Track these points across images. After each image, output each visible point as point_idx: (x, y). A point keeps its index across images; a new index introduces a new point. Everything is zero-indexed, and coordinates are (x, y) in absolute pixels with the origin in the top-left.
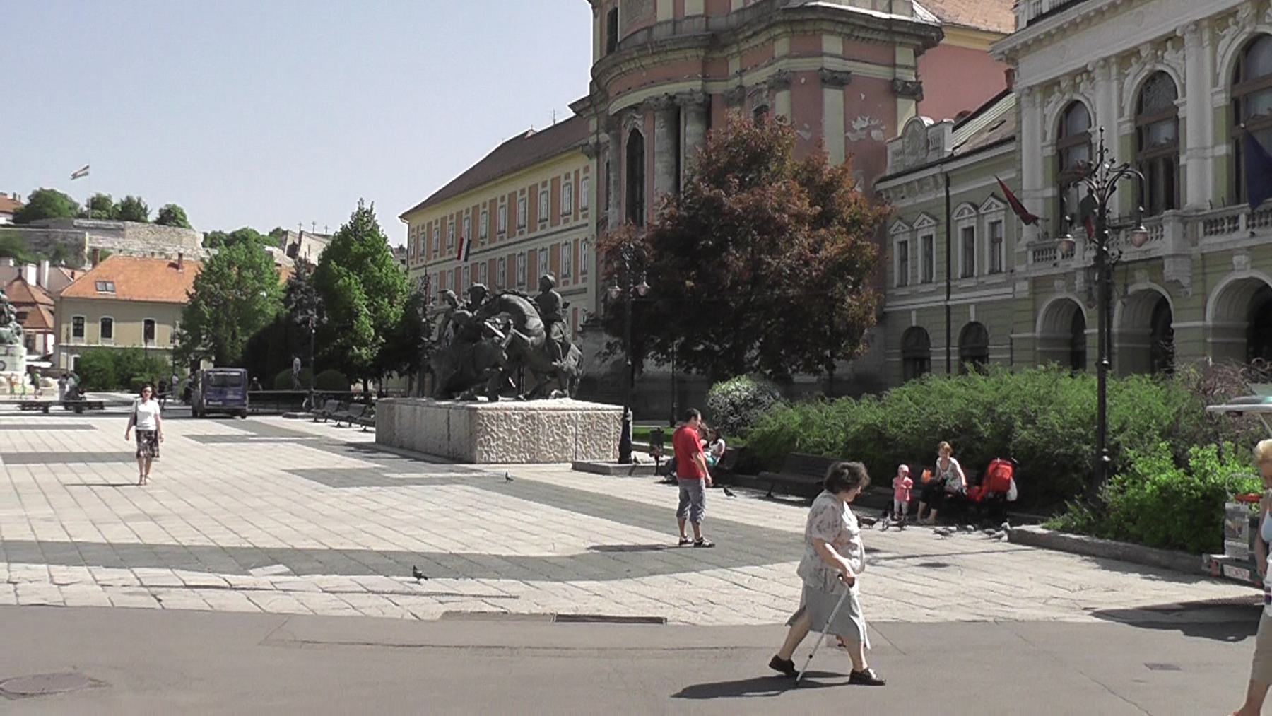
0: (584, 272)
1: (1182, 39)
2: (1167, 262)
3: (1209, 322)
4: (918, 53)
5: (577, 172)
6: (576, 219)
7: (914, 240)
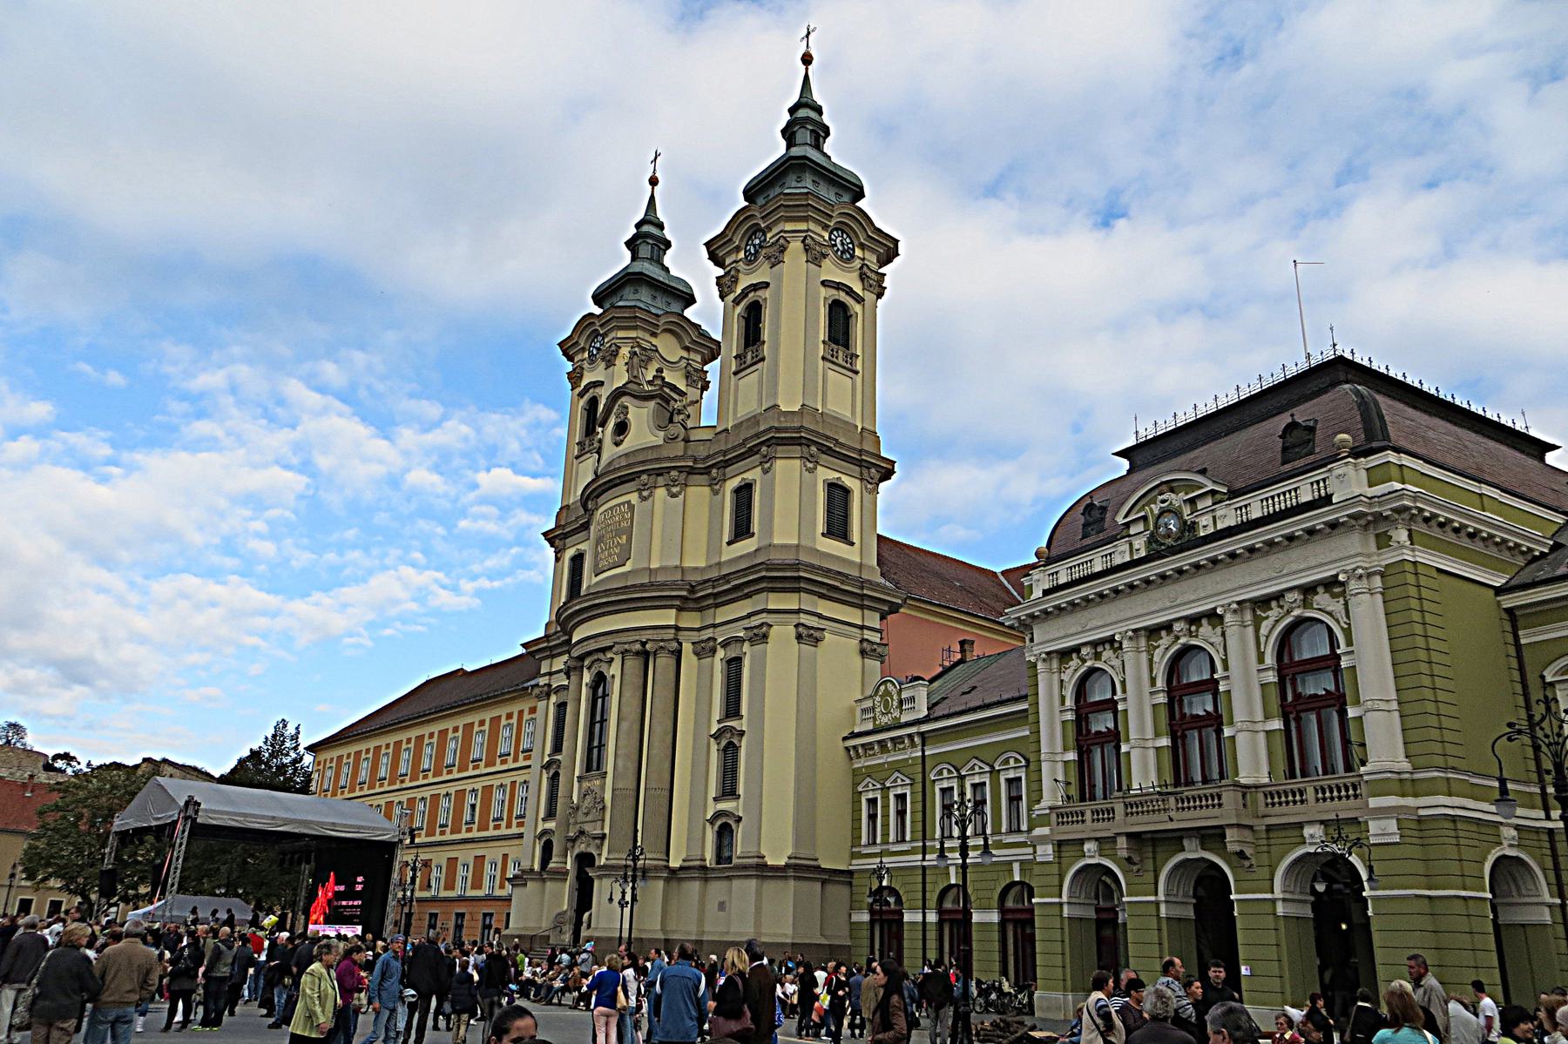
0: (522, 816)
1: (1221, 617)
2: (1228, 832)
3: (1065, 899)
4: (883, 618)
5: (521, 713)
6: (516, 760)
7: (886, 798)
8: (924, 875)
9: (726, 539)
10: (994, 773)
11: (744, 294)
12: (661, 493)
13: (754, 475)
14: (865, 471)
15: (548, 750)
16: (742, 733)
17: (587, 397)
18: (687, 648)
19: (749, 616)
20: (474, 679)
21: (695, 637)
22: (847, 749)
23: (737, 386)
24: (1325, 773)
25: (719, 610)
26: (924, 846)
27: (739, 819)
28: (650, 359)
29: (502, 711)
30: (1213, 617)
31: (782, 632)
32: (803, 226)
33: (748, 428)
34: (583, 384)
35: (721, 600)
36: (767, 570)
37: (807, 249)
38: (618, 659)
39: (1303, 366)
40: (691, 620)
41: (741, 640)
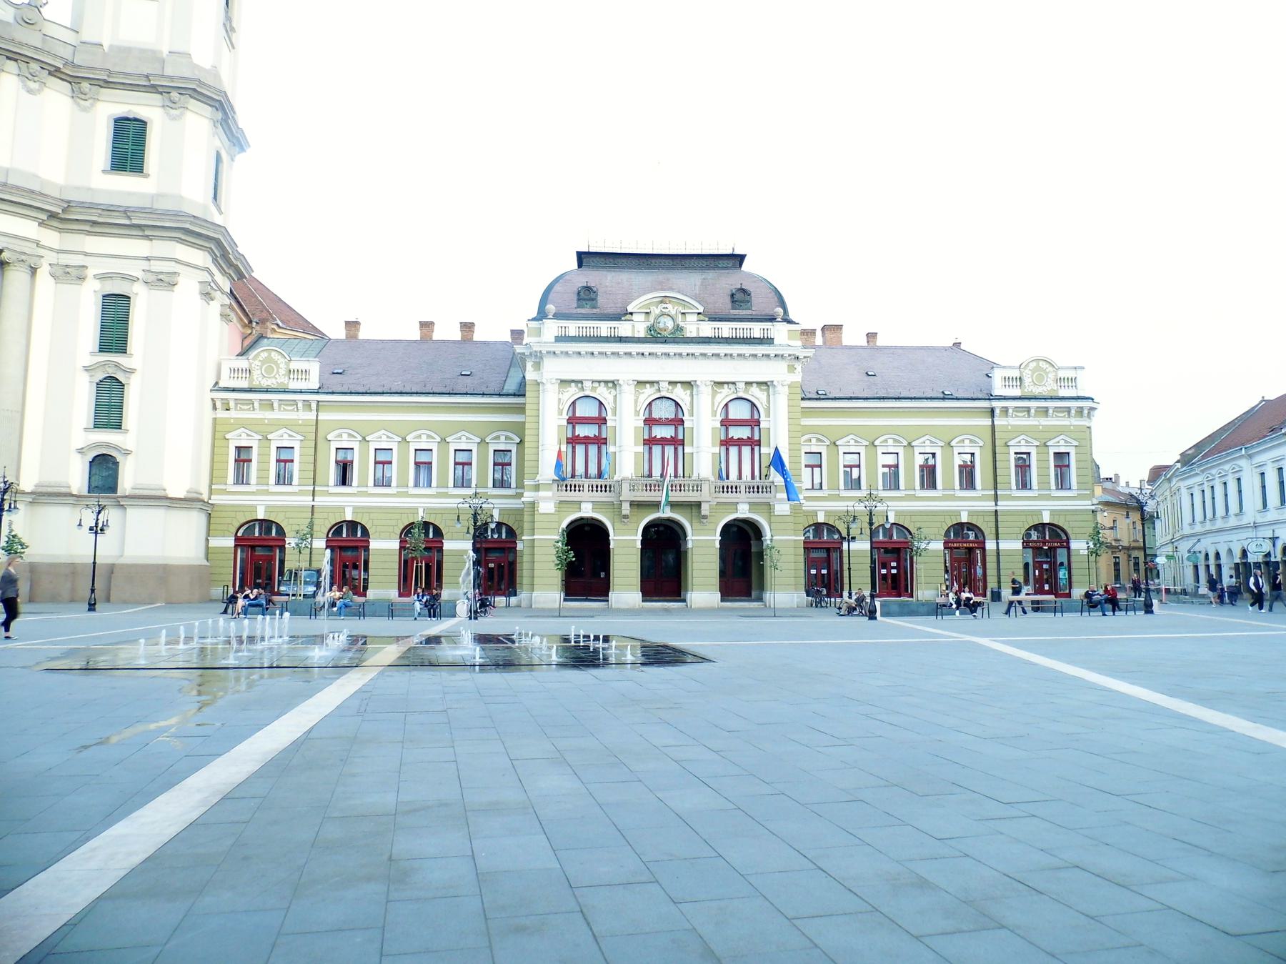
16: (131, 371)
24: (278, 483)
26: (996, 495)
30: (614, 384)
36: (191, 223)
39: (729, 252)
40: (50, 237)
41: (133, 279)
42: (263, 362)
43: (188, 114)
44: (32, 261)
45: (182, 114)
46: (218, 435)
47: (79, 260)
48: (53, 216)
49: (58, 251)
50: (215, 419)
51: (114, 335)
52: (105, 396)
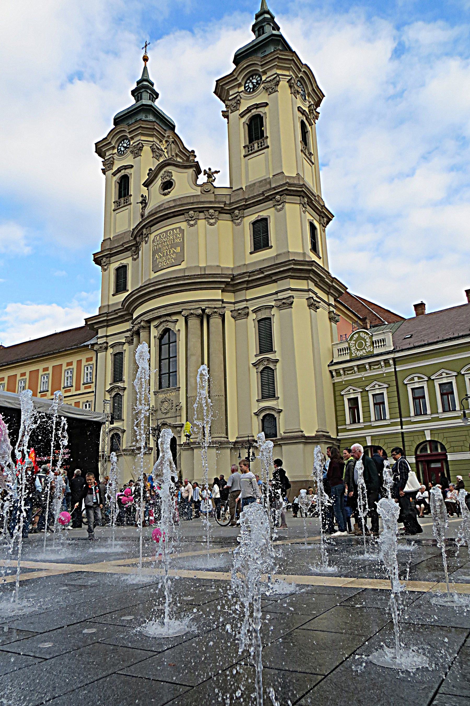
5: (79, 362)
6: (78, 389)
8: (403, 437)
9: (112, 293)
10: (365, 392)
11: (119, 171)
12: (202, 223)
13: (128, 261)
14: (321, 219)
15: (109, 379)
16: (277, 361)
17: (119, 175)
18: (228, 314)
19: (276, 293)
20: (8, 350)
21: (232, 307)
22: (331, 372)
23: (247, 165)
25: (109, 328)
26: (401, 421)
27: (124, 431)
28: (161, 155)
29: (63, 361)
31: (300, 302)
32: (151, 139)
33: (260, 187)
34: (115, 169)
35: (251, 284)
36: (295, 264)
37: (153, 151)
38: (182, 320)
40: (229, 297)
42: (356, 341)
43: (287, 205)
44: (220, 311)
45: (283, 206)
46: (337, 393)
47: (243, 305)
48: (227, 283)
49: (234, 303)
50: (334, 384)
51: (266, 344)
52: (265, 379)
